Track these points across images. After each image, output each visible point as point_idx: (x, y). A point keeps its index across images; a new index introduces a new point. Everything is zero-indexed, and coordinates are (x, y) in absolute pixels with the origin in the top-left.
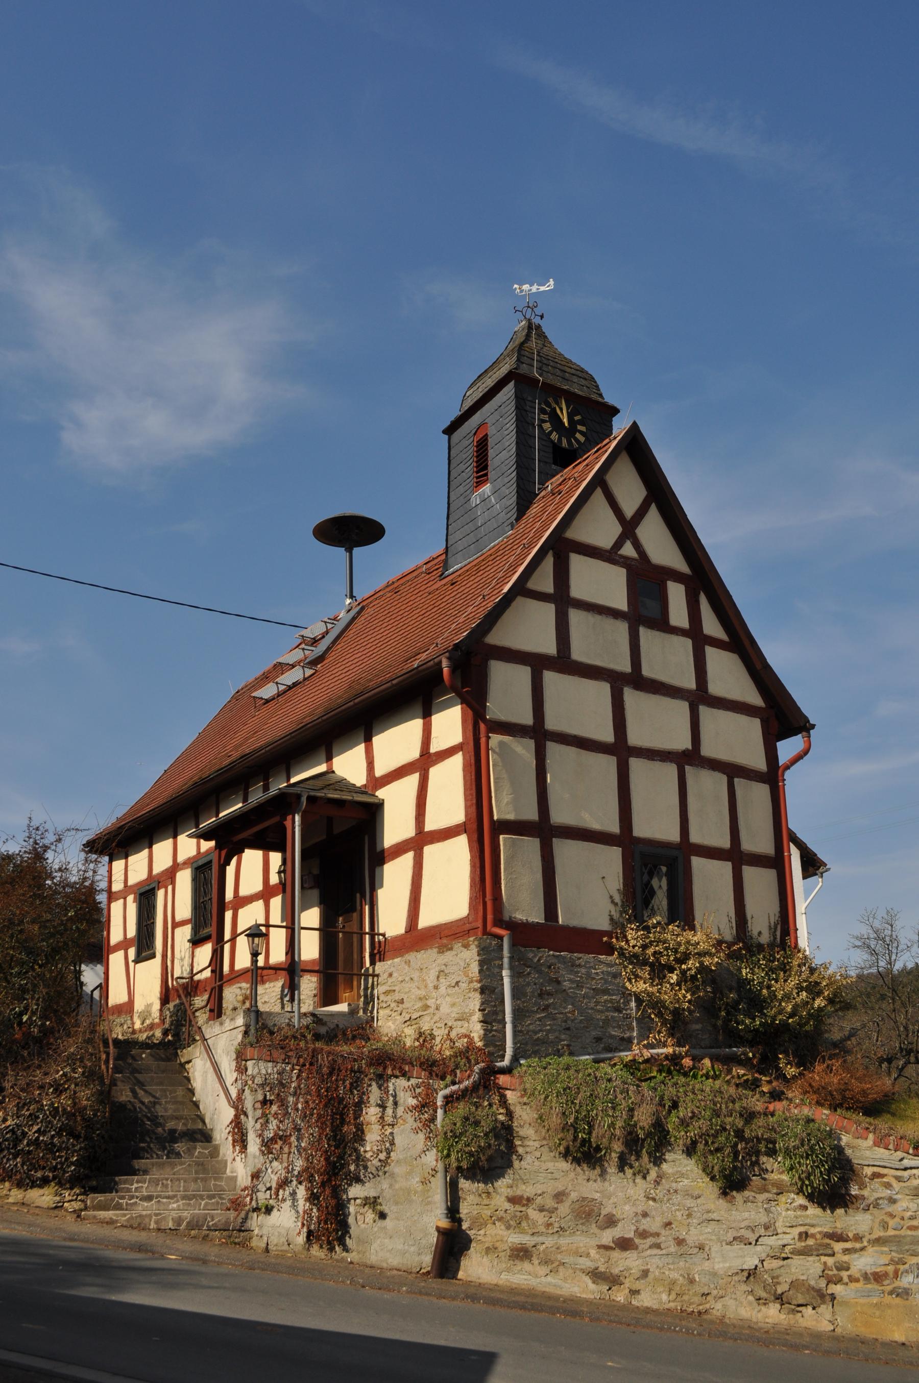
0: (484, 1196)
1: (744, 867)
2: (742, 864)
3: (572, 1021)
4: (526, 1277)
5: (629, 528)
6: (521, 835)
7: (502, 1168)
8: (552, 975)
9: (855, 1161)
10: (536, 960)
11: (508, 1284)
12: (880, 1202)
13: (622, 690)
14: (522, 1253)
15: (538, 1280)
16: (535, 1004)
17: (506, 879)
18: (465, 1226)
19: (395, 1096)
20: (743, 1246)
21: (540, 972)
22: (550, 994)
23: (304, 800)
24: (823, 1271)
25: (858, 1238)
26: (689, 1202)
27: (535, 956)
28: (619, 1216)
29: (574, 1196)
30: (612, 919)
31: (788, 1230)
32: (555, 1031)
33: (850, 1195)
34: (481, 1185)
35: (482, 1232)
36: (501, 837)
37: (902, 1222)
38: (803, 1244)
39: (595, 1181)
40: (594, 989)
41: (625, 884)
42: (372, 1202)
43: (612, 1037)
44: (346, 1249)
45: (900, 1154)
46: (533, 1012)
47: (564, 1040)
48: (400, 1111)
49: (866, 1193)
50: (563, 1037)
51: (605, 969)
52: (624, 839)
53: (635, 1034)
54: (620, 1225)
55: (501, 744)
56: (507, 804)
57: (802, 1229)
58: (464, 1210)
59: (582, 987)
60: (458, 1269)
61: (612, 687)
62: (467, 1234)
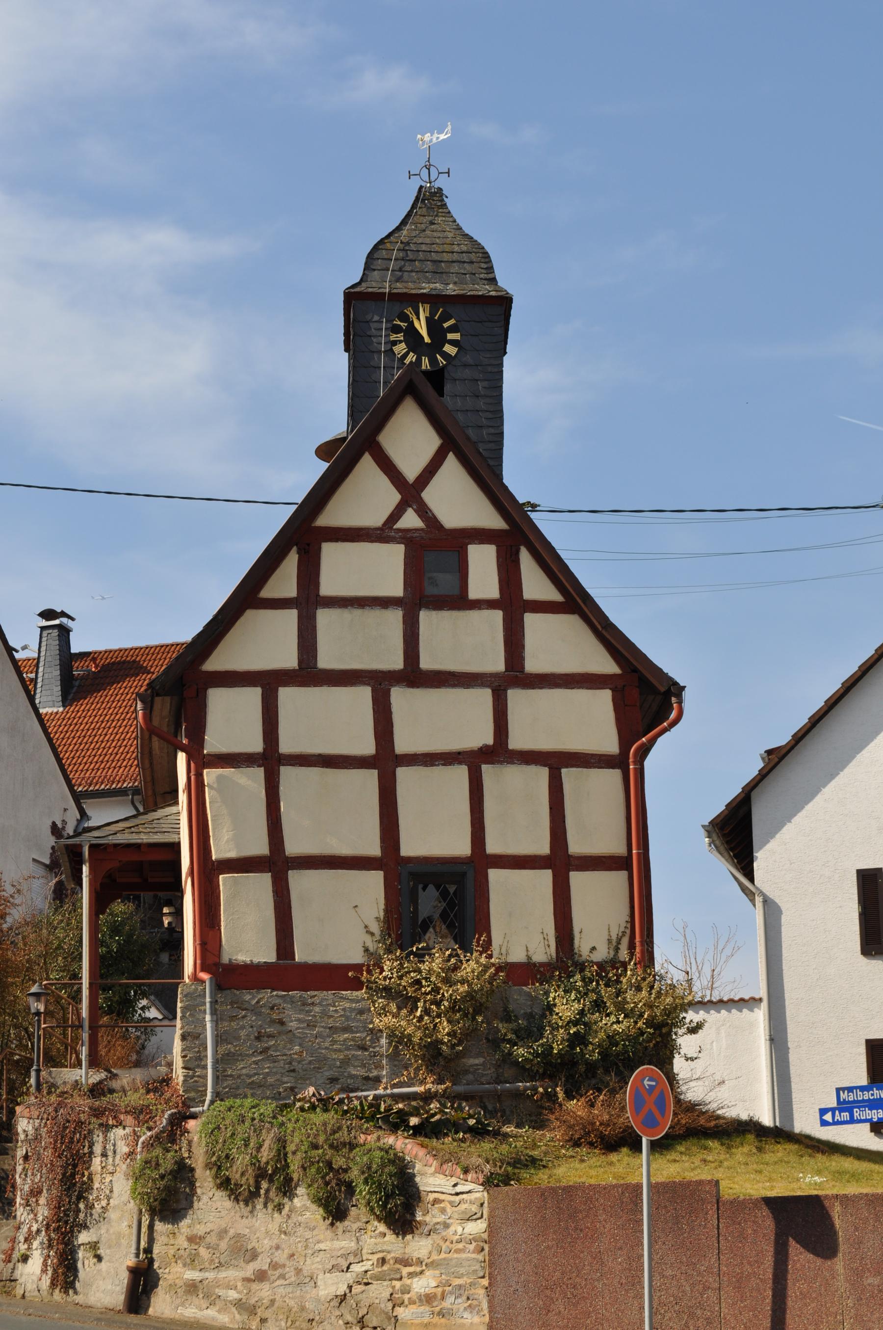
0: (171, 1236)
1: (572, 874)
2: (569, 871)
3: (299, 1062)
4: (193, 1311)
5: (411, 493)
6: (247, 872)
7: (186, 1209)
8: (275, 1016)
9: (421, 1188)
10: (254, 1002)
11: (182, 1318)
12: (438, 1227)
13: (389, 690)
14: (192, 1288)
15: (202, 1313)
16: (250, 1047)
17: (226, 921)
18: (156, 1266)
19: (114, 1145)
20: (338, 1274)
21: (258, 1014)
22: (270, 1036)
23: (86, 850)
24: (391, 1294)
25: (420, 1262)
26: (308, 1235)
27: (253, 998)
28: (259, 1250)
29: (232, 1232)
30: (366, 950)
31: (370, 1257)
32: (276, 1073)
33: (416, 1221)
34: (170, 1226)
35: (167, 1271)
36: (221, 876)
37: (451, 1246)
38: (380, 1270)
39: (247, 1217)
40: (330, 1028)
41: (387, 911)
42: (94, 1246)
43: (351, 1076)
44: (76, 1293)
45: (454, 1180)
46: (247, 1055)
47: (287, 1083)
48: (118, 1157)
49: (427, 1219)
50: (285, 1079)
51: (347, 1005)
52: (390, 860)
53: (384, 1073)
54: (259, 1258)
55: (219, 778)
56: (227, 841)
57: (380, 1255)
58: (156, 1250)
59: (315, 1026)
60: (148, 1306)
61: (373, 691)
62: (157, 1273)
